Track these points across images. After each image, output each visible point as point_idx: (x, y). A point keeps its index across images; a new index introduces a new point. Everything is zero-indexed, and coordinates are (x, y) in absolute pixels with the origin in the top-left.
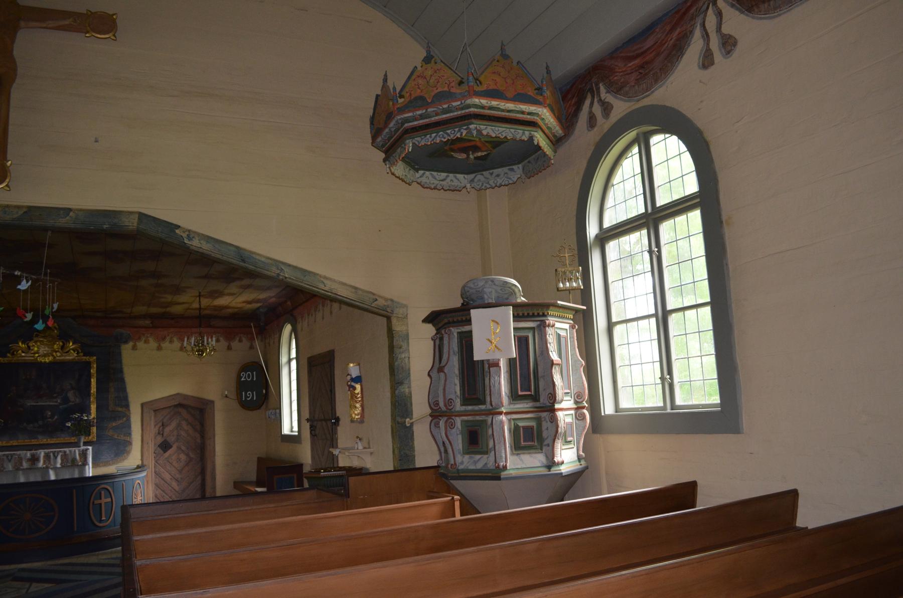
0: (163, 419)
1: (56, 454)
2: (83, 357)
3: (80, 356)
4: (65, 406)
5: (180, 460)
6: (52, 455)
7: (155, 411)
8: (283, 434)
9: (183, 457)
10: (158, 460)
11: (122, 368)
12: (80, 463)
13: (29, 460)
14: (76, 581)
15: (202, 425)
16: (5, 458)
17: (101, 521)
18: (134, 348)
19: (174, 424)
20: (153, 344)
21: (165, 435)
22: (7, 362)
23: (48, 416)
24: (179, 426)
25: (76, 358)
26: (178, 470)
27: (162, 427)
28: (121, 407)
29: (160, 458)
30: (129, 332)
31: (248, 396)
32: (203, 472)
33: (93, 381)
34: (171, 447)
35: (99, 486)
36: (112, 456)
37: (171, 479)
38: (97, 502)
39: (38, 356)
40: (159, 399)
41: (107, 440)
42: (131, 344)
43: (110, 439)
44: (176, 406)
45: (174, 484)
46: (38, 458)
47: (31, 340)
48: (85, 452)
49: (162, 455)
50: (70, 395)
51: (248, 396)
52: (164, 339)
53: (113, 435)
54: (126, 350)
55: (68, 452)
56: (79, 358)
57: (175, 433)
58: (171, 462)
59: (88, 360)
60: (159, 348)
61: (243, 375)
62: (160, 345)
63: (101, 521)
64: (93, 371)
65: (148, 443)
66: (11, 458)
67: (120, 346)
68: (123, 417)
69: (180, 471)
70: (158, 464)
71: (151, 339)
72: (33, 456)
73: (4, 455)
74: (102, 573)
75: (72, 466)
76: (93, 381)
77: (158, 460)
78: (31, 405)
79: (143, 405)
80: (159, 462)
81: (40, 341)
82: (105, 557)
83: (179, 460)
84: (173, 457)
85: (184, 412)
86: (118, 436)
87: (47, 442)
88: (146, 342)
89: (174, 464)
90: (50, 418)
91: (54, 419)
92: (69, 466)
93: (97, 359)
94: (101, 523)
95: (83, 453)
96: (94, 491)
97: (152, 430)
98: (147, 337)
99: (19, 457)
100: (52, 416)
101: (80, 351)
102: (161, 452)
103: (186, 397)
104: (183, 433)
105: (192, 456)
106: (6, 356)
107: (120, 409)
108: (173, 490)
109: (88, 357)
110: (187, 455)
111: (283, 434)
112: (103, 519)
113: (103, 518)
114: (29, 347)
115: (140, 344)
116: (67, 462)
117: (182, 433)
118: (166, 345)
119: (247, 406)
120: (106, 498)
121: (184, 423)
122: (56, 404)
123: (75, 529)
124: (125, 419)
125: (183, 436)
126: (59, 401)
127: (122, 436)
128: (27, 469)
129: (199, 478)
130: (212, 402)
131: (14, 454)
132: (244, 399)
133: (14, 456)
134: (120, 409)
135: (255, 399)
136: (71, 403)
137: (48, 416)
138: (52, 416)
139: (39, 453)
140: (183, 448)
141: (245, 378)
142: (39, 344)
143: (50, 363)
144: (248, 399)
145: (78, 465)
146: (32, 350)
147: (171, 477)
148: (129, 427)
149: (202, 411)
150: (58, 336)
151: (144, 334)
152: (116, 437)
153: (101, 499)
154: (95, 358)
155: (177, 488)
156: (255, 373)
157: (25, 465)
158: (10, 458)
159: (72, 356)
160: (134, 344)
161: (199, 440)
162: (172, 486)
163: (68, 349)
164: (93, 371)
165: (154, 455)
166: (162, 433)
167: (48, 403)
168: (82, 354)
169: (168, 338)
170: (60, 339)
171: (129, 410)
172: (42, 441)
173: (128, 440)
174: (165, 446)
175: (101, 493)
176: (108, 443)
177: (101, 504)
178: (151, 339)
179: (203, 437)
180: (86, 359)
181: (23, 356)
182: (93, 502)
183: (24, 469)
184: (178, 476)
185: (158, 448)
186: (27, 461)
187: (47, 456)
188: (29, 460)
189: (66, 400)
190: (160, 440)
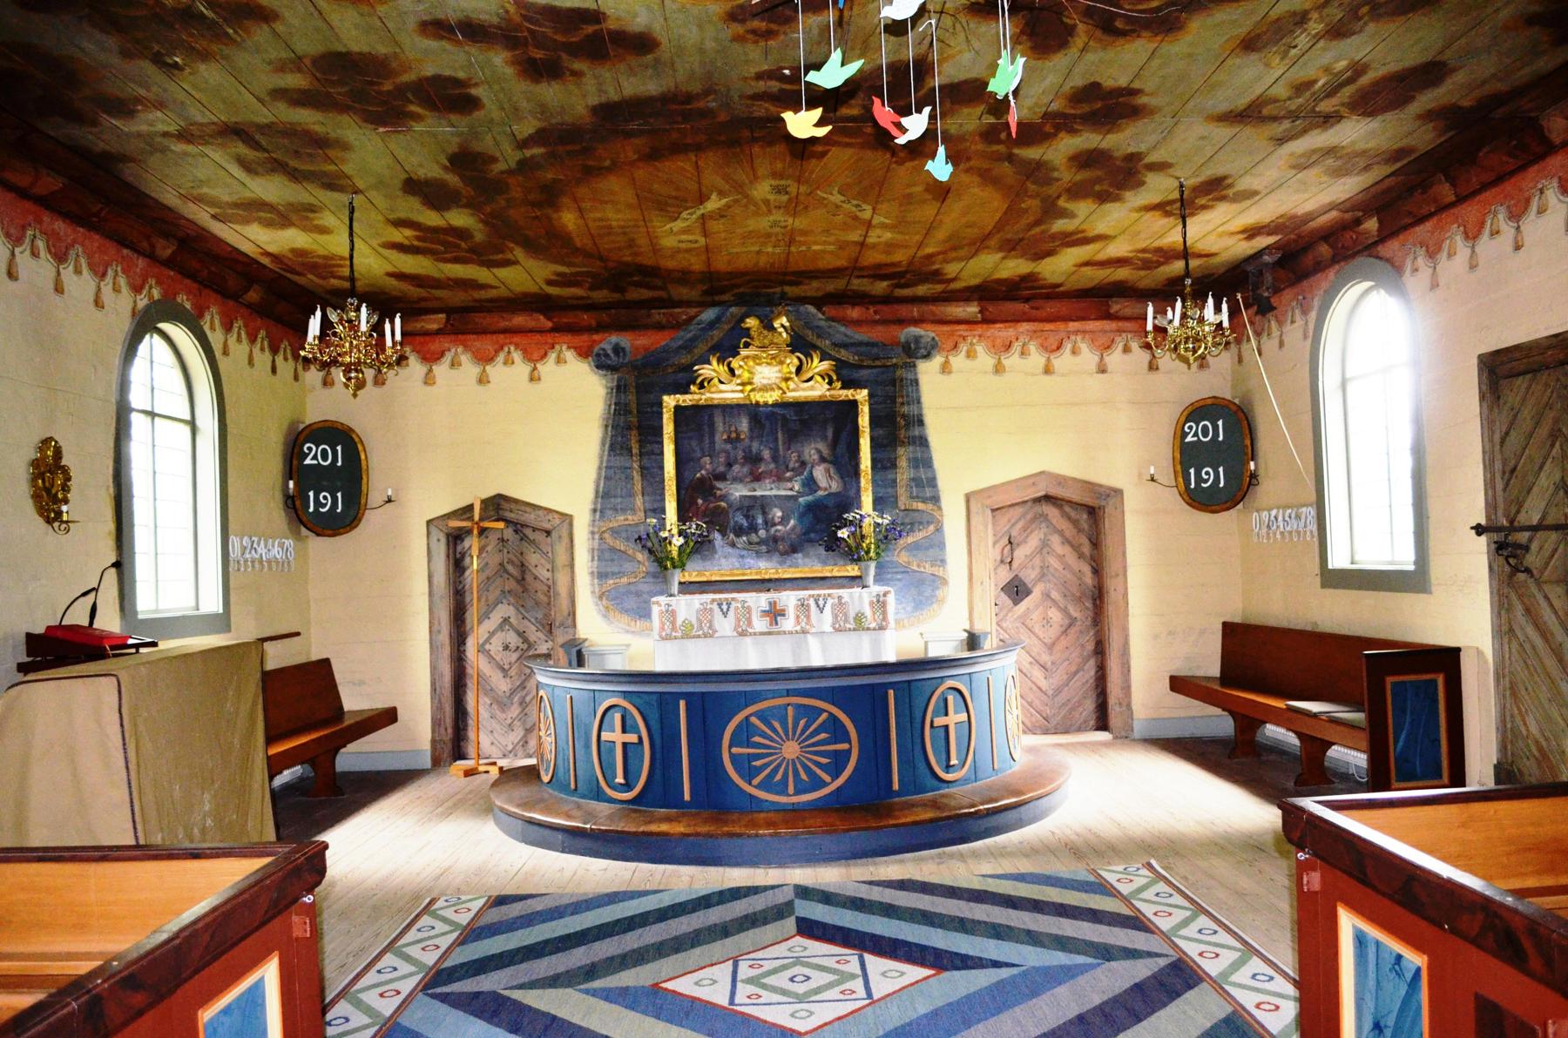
0: (1008, 531)
1: (821, 603)
2: (841, 392)
3: (834, 389)
4: (810, 498)
5: (1048, 622)
6: (812, 602)
7: (993, 510)
8: (1330, 567)
9: (1055, 615)
10: (1001, 620)
11: (921, 415)
12: (873, 625)
13: (765, 613)
14: (996, 964)
15: (1096, 544)
16: (715, 606)
17: (948, 767)
18: (945, 369)
19: (1033, 542)
20: (985, 359)
21: (1015, 565)
22: (690, 403)
23: (777, 520)
24: (1045, 545)
25: (828, 393)
26: (1045, 644)
27: (1009, 547)
28: (923, 502)
29: (1007, 614)
30: (933, 335)
31: (1206, 477)
32: (1100, 650)
33: (865, 444)
34: (1028, 593)
35: (941, 684)
36: (909, 609)
37: (1031, 663)
38: (939, 721)
39: (753, 390)
40: (1003, 484)
41: (897, 573)
42: (938, 360)
43: (903, 572)
44: (1037, 500)
45: (1037, 674)
46: (784, 610)
47: (735, 354)
48: (881, 599)
49: (1010, 611)
50: (819, 473)
51: (1206, 477)
52: (1008, 347)
53: (909, 563)
54: (928, 372)
55: (846, 599)
56: (833, 392)
57: (1037, 561)
58: (1030, 626)
59: (851, 398)
60: (999, 369)
61: (1190, 428)
62: (999, 362)
63: (948, 767)
64: (864, 420)
65: (982, 583)
66: (728, 610)
67: (915, 366)
68: (929, 523)
69: (1050, 647)
70: (1001, 628)
71: (980, 349)
72: (773, 604)
73: (713, 600)
74: (1062, 943)
75: (854, 630)
76: (865, 444)
77: (1001, 620)
78: (741, 497)
79: (968, 498)
80: (1004, 625)
81: (755, 358)
82: (987, 868)
83: (1047, 621)
84: (1035, 616)
85: (1051, 511)
86: (919, 566)
87: (776, 576)
88: (971, 355)
89: (1036, 630)
90: (779, 523)
91: (788, 527)
92: (850, 630)
93: (871, 395)
94: (947, 773)
95: (878, 601)
96: (932, 694)
97: (989, 552)
98: (972, 344)
99: (743, 607)
100: (784, 521)
101: (835, 378)
102: (1009, 602)
103: (1061, 480)
104: (1053, 562)
105: (1075, 614)
106: (686, 391)
107: (921, 506)
108: (1034, 688)
109: (852, 391)
110: (1065, 611)
111: (1330, 567)
112: (952, 763)
113: (954, 761)
114: (732, 371)
115: (958, 361)
116: (846, 621)
117: (1052, 562)
118: (1012, 360)
119: (1203, 500)
120: (956, 712)
121: (1056, 541)
122: (790, 493)
123: (896, 786)
124: (932, 528)
125: (1056, 569)
126: (797, 488)
127: (927, 566)
128: (762, 634)
129: (1092, 663)
130: (1118, 492)
131: (733, 599)
132: (1193, 486)
133: (734, 605)
134: (921, 506)
135: (1222, 485)
136: (821, 493)
137: (777, 520)
138: (784, 521)
139: (785, 598)
140: (1055, 595)
141: (1196, 435)
142: (751, 363)
143: (776, 405)
144: (1204, 485)
145: (868, 629)
146: (739, 376)
147: (1031, 660)
148: (941, 545)
149: (1093, 512)
150: (788, 346)
151: (964, 338)
152: (915, 568)
153: (946, 714)
154: (865, 392)
155: (1044, 684)
156: (1220, 423)
157: (760, 624)
158: (725, 607)
159: (817, 390)
160: (943, 359)
161: (1089, 579)
162: (1034, 680)
163: (809, 375)
164: (864, 420)
165: (995, 609)
166: (1009, 560)
167: (774, 492)
168: (839, 385)
169: (1017, 346)
170: (792, 352)
171: (940, 508)
172: (766, 573)
173: (941, 574)
174: (1016, 590)
175: (946, 700)
176: (899, 580)
177: (946, 727)
178: (980, 349)
179: (1097, 571)
180: (847, 396)
181: (728, 393)
182: (932, 722)
183: (755, 634)
184: (1046, 658)
185: (1002, 594)
186: (761, 617)
187: (803, 605)
188: (765, 613)
189: (811, 484)
190: (1005, 576)
